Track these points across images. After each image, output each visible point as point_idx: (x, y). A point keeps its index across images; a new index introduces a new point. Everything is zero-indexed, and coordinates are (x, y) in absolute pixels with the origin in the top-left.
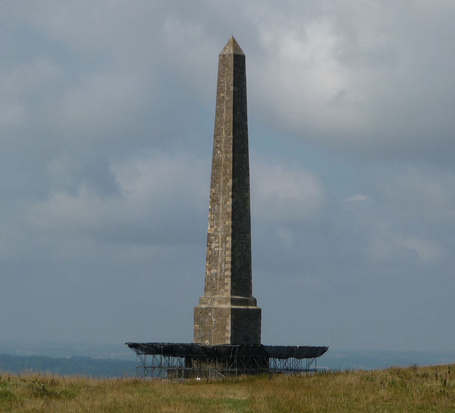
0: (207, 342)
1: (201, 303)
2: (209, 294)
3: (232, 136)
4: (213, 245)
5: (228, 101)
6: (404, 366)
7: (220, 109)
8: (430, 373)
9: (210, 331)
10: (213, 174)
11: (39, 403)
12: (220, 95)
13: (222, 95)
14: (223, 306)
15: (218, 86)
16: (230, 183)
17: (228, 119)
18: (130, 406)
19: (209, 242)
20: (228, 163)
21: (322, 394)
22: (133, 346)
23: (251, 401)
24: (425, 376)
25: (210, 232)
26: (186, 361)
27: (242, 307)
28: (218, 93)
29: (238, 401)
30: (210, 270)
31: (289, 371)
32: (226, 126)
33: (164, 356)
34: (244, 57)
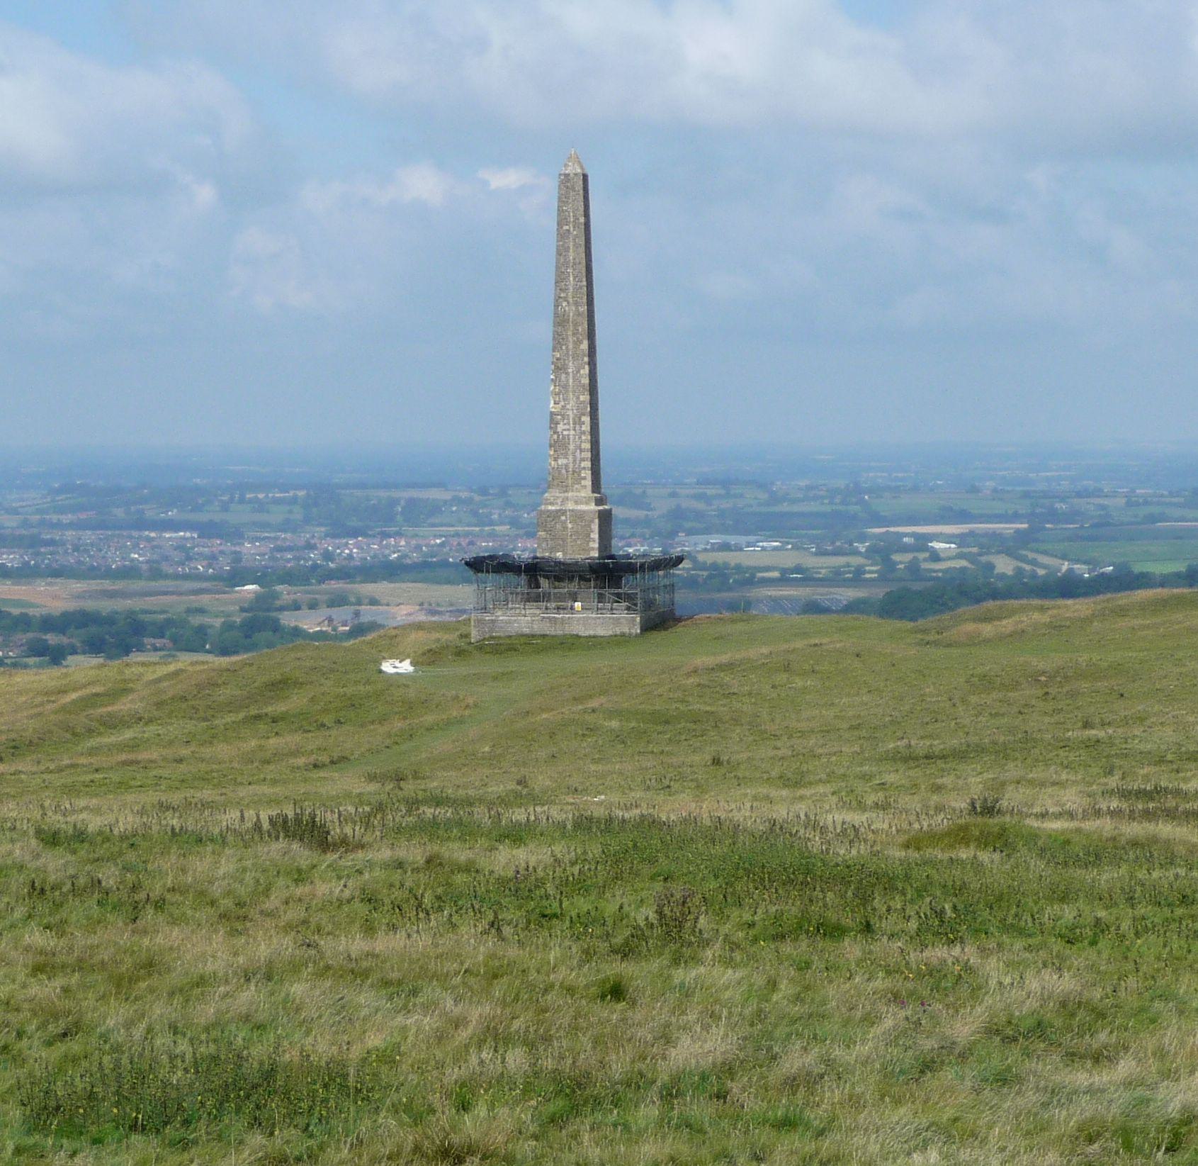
0: (559, 555)
3: (585, 283)
4: (560, 428)
5: (576, 236)
7: (563, 246)
9: (563, 540)
10: (556, 333)
12: (562, 228)
13: (566, 228)
14: (583, 507)
15: (559, 215)
17: (577, 261)
19: (553, 423)
20: (579, 319)
21: (689, 622)
25: (553, 410)
28: (560, 224)
30: (556, 460)
32: (574, 270)
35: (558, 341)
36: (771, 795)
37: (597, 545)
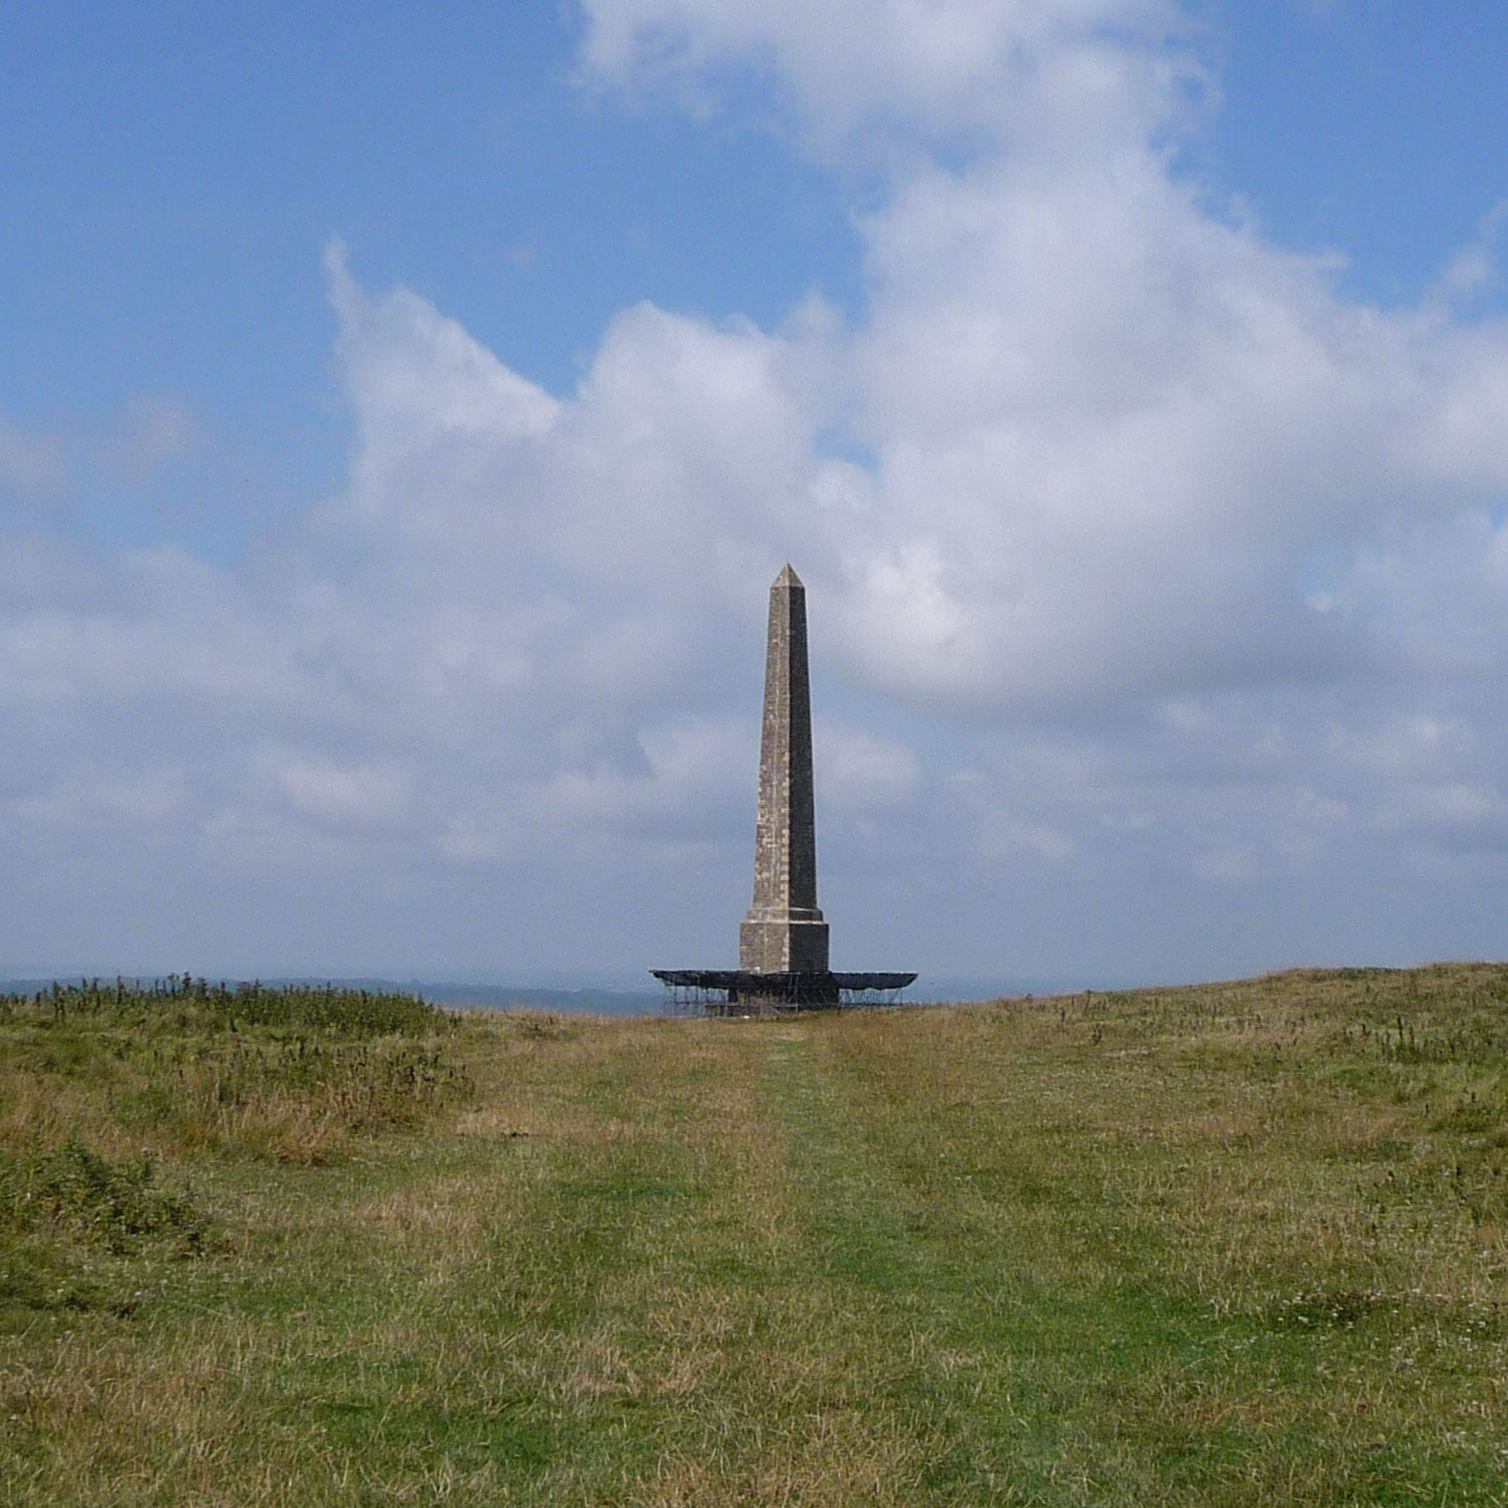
1: (749, 918)
2: (759, 906)
3: (788, 696)
4: (765, 840)
5: (783, 648)
6: (1014, 998)
8: (1050, 1004)
11: (529, 1047)
14: (779, 921)
16: (787, 758)
18: (648, 1050)
22: (658, 974)
23: (808, 1044)
24: (1042, 1008)
26: (729, 994)
27: (803, 922)
29: (791, 1043)
30: (760, 873)
31: (1413, 1328)
33: (702, 987)
34: (803, 590)
35: (766, 753)
36: (20, 1394)
37: (787, 960)
